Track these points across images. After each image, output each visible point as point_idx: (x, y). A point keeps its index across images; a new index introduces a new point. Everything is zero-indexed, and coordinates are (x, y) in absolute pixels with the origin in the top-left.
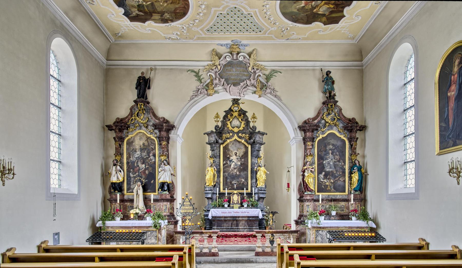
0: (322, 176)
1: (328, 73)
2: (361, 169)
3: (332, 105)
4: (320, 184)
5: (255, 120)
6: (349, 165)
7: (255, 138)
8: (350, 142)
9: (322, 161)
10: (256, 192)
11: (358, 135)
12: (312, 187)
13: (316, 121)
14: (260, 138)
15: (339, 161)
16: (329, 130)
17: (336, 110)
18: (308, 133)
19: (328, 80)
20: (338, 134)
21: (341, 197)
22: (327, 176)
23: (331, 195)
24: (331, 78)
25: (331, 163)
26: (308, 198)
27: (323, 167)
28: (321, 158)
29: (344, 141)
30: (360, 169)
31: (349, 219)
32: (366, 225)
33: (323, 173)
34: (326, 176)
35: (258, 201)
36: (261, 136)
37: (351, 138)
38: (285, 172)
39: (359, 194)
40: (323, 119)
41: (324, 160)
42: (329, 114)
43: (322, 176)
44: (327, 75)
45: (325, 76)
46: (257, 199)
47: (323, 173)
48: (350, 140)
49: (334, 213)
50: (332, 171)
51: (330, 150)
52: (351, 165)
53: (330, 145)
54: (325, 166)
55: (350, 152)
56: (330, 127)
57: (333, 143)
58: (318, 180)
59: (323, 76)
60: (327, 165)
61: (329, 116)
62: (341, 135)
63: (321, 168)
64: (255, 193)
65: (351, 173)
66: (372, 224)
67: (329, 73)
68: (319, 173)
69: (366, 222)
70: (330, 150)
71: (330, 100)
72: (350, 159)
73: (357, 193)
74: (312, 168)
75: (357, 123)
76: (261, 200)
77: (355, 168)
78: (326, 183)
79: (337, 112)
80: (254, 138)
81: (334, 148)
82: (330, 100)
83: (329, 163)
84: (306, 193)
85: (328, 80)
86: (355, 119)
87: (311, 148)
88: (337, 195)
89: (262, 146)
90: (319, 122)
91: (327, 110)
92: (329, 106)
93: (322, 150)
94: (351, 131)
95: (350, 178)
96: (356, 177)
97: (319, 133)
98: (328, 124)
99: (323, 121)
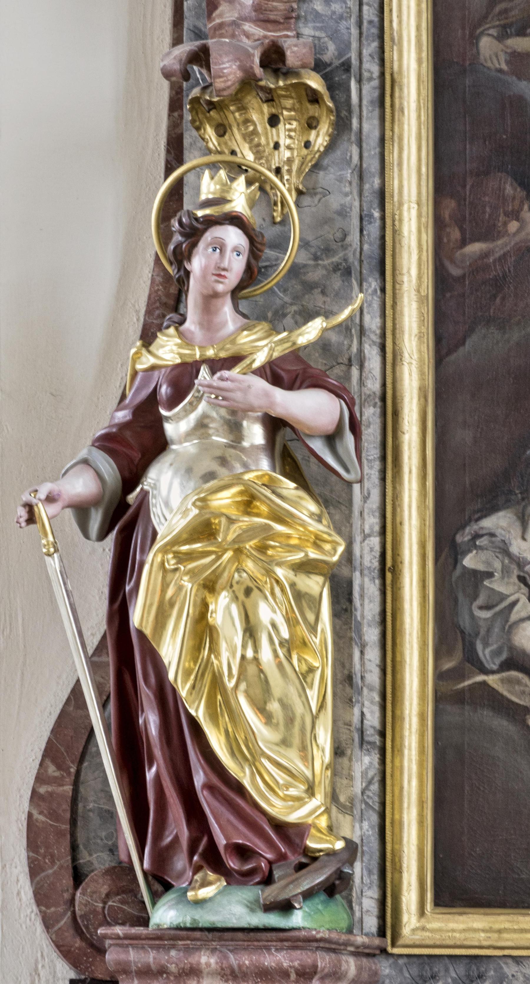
12: (288, 775)
58: (451, 634)
74: (285, 373)
84: (165, 914)
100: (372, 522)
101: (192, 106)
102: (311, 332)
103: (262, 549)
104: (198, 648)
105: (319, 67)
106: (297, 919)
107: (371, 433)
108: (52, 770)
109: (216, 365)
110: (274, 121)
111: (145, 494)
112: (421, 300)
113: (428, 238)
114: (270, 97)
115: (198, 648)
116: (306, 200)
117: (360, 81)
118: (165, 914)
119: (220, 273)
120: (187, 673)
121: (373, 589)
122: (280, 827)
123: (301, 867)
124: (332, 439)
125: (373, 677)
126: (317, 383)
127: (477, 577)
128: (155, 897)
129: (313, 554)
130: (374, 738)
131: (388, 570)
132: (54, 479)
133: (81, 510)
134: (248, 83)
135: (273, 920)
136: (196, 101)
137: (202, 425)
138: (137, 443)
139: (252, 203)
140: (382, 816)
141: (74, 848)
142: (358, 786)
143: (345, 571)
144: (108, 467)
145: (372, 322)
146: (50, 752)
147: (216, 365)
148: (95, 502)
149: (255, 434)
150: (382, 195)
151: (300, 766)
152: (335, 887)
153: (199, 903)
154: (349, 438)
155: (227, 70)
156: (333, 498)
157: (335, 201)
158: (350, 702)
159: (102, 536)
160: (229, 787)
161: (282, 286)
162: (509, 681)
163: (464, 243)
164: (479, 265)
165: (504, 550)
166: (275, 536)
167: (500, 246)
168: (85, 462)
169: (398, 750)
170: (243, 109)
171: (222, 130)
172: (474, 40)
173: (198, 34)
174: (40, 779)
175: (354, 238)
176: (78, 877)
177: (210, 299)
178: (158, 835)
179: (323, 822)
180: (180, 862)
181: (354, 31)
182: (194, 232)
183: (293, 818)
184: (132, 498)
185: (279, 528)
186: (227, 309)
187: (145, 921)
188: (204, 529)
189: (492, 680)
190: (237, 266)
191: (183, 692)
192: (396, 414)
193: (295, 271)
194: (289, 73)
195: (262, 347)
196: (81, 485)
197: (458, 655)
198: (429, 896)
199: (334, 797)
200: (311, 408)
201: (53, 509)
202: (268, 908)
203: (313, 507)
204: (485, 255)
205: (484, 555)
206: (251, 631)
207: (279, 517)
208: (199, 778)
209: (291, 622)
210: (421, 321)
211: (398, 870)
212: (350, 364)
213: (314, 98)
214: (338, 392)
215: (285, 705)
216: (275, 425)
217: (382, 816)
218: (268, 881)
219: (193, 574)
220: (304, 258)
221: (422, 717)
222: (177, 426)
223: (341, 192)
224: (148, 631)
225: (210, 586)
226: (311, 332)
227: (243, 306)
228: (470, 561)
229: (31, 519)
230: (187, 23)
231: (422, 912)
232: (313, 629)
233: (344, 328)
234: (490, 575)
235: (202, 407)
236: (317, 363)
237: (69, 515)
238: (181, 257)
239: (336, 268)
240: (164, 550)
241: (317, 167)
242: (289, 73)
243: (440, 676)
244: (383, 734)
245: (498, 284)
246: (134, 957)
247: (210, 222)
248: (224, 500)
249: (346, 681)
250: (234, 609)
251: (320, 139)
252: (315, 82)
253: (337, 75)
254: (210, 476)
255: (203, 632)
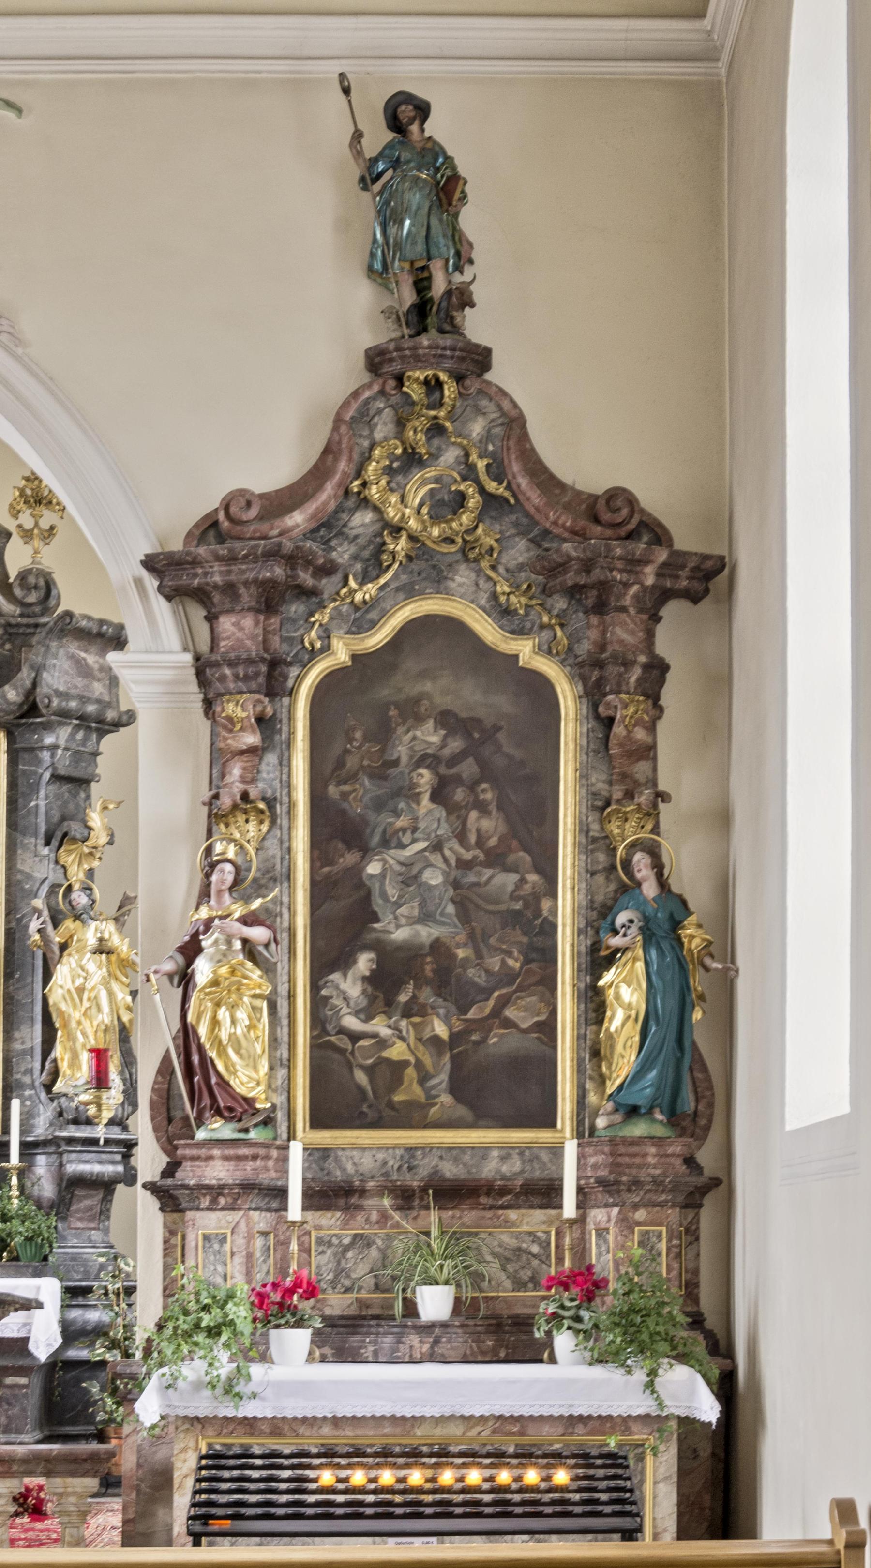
0: (350, 985)
1: (405, 113)
2: (676, 924)
3: (433, 386)
4: (330, 1053)
5: (48, 518)
6: (590, 891)
7: (38, 669)
8: (593, 694)
9: (350, 858)
10: (41, 1129)
11: (675, 635)
12: (247, 1078)
13: (298, 519)
14: (84, 671)
15: (496, 859)
16: (409, 592)
17: (477, 428)
18: (226, 623)
19: (408, 170)
20: (487, 630)
21: (513, 1166)
22: (397, 986)
23: (427, 1150)
24: (433, 154)
25: (434, 878)
26: (218, 1171)
27: (363, 913)
28: (338, 831)
29: (540, 690)
30: (664, 927)
31: (537, 1352)
32: (642, 1405)
33: (364, 962)
34: (383, 988)
35: (60, 1207)
36: (91, 659)
37: (599, 664)
38: (29, 959)
39: (653, 1140)
40: (364, 502)
41: (366, 852)
42: (412, 460)
43: (350, 985)
44: (395, 123)
45: (378, 136)
46: (47, 1190)
47: (364, 962)
48: (596, 677)
49: (434, 1303)
50: (437, 947)
51: (423, 760)
52: (605, 889)
53: (419, 719)
54: (377, 903)
55: (599, 782)
56: (427, 568)
57: (444, 702)
58: (318, 1021)
59: (358, 136)
60: (392, 892)
61: (417, 476)
62: (519, 632)
63: (343, 922)
64: (28, 1148)
65: (598, 960)
66: (693, 1392)
67: (406, 111)
68: (327, 961)
69: (640, 1376)
70: (423, 760)
71: (427, 334)
72: (594, 842)
73: (639, 1129)
74: (248, 920)
75: (658, 534)
76: (88, 1201)
77: (622, 918)
78: (382, 1043)
79: (488, 437)
80: (25, 676)
81: (456, 745)
82: (427, 334)
83: (410, 878)
84: (201, 1135)
85: (408, 170)
86: (631, 501)
87: (252, 750)
88: (483, 1152)
89: (109, 742)
90: (328, 527)
91: (401, 423)
92: (415, 392)
93: (352, 762)
94: (596, 599)
95: (594, 1005)
96: (627, 990)
97: (322, 617)
98: (402, 545)
99: (362, 520)
100: (285, 978)
101: (217, 817)
102: (256, 904)
103: (238, 989)
104: (213, 1030)
105: (264, 799)
106: (253, 1135)
107: (285, 943)
108: (160, 1079)
109: (221, 918)
110: (247, 821)
111: (193, 970)
112: (305, 890)
113: (308, 866)
114: (245, 812)
115: (213, 1030)
116: (260, 852)
117: (281, 804)
118: (201, 1135)
119: (223, 882)
120: (209, 1039)
121: (285, 1004)
122: (245, 1099)
123: (253, 1114)
124: (267, 946)
125: (286, 1039)
126: (260, 923)
127: (327, 999)
128: (198, 1127)
129: (258, 991)
130: (285, 1062)
131: (291, 996)
132: (158, 964)
133: (170, 976)
134: (235, 807)
135: (242, 1136)
136: (216, 814)
137: (216, 942)
138: (191, 949)
139: (236, 854)
140: (289, 1092)
141: (168, 1110)
142: (279, 1082)
143: (274, 998)
144: (180, 959)
145: (285, 899)
146: (160, 1072)
147: (221, 918)
148: (176, 973)
149: (238, 945)
150: (289, 850)
151: (254, 1075)
152: (268, 1121)
153: (213, 1130)
154: (273, 945)
155: (226, 802)
156: (269, 969)
157: (271, 852)
158: (276, 1049)
159: (179, 986)
160: (224, 1084)
161: (250, 886)
162: (341, 1039)
163: (322, 867)
164: (328, 876)
165: (337, 987)
166: (243, 985)
167: (335, 869)
168: (171, 957)
169: (295, 1067)
170: (234, 817)
171: (227, 825)
172: (326, 786)
173: (218, 787)
174: (155, 1082)
175: (278, 867)
176: (170, 1120)
177: (220, 892)
178: (199, 1104)
179: (263, 1096)
180: (207, 1114)
181: (279, 785)
182: (213, 866)
183: (251, 1095)
184: (189, 970)
185: (245, 981)
186: (227, 897)
187: (193, 1138)
188: (215, 983)
189: (333, 1039)
190: (230, 879)
191: (207, 1046)
192: (295, 935)
193: (255, 880)
194: (251, 802)
195: (238, 910)
196: (169, 966)
197: (319, 1028)
198: (308, 1124)
199: (269, 1086)
200: (258, 934)
201: (158, 976)
202: (240, 1131)
203: (259, 972)
204: (330, 872)
205: (330, 990)
206: (234, 1022)
207: (246, 977)
208: (214, 1080)
209: (249, 1017)
210: (305, 899)
211: (295, 1115)
212: (276, 916)
213: (262, 812)
214: (269, 927)
215: (248, 1051)
216: (245, 941)
217: (289, 1092)
218: (240, 1120)
219: (211, 1000)
220: (259, 875)
221: (305, 1053)
222: (206, 942)
223: (273, 848)
224: (194, 1023)
225: (218, 1005)
226: (256, 904)
227: (234, 895)
228: (324, 992)
229: (148, 980)
230: (214, 783)
231: (304, 1131)
232: (259, 1020)
233: (274, 901)
234: (331, 997)
235: (216, 935)
236: (263, 916)
237: (165, 978)
238: (208, 875)
239: (271, 879)
240: (200, 991)
241: (264, 839)
242: (251, 802)
243: (312, 1038)
244: (289, 1060)
245: (335, 884)
246: (188, 1152)
247: (219, 862)
248: (224, 971)
249: (274, 1041)
250: (227, 1014)
251: (265, 828)
252: (262, 805)
253: (271, 802)
254: (219, 961)
255: (215, 1023)
